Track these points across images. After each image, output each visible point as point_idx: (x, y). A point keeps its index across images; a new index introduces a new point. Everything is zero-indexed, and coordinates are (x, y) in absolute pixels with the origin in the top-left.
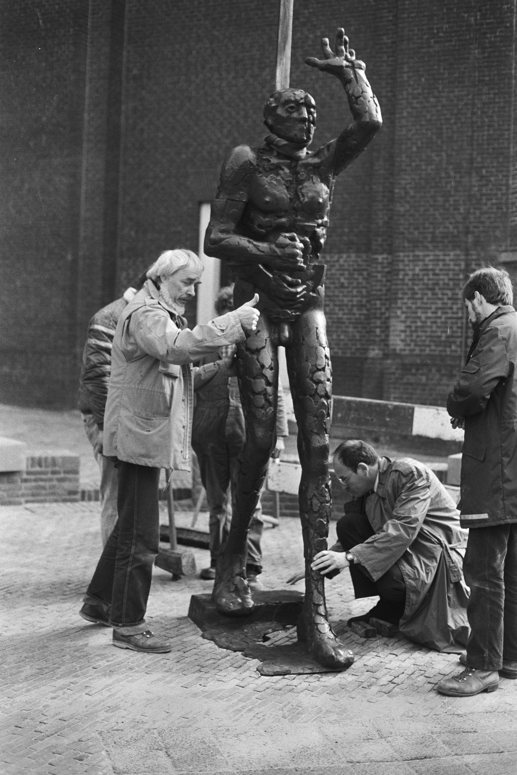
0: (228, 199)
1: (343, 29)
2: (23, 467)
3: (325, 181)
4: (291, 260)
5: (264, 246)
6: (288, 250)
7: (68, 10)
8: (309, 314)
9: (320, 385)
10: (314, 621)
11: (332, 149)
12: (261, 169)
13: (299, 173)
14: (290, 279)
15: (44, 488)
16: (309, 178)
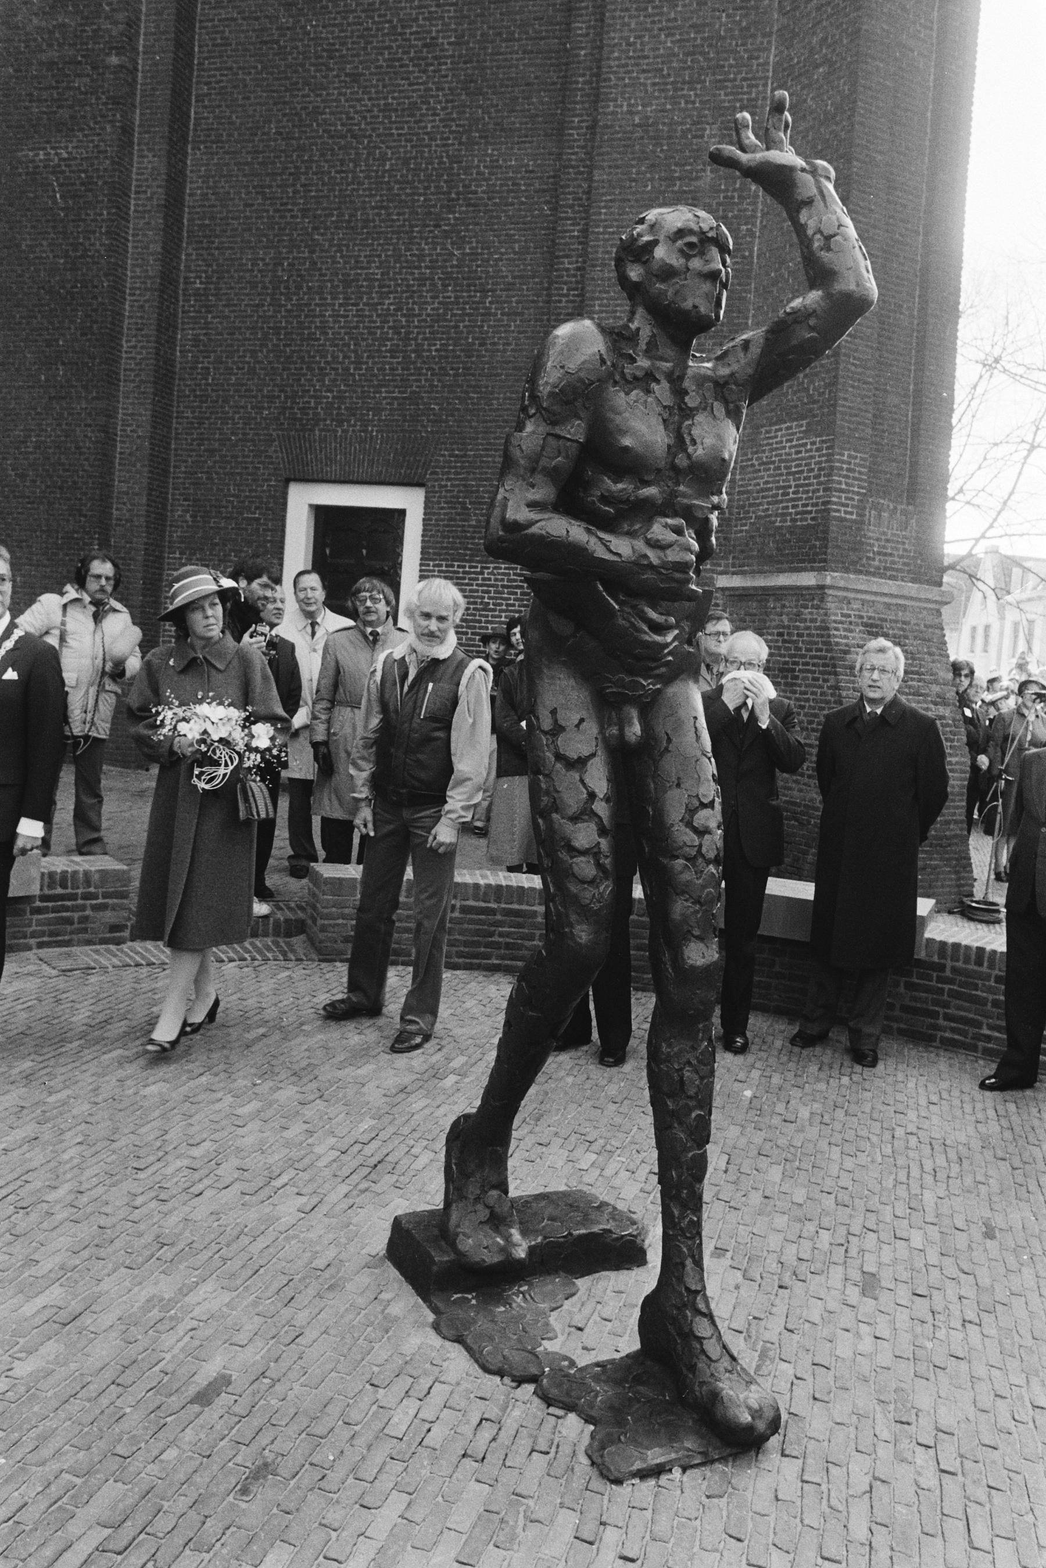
0: (548, 434)
2: (35, 890)
3: (734, 414)
4: (677, 575)
6: (672, 556)
7: (100, 183)
8: (672, 690)
9: (707, 837)
10: (691, 1331)
11: (755, 350)
12: (617, 378)
13: (687, 393)
14: (653, 615)
15: (69, 921)
16: (704, 407)
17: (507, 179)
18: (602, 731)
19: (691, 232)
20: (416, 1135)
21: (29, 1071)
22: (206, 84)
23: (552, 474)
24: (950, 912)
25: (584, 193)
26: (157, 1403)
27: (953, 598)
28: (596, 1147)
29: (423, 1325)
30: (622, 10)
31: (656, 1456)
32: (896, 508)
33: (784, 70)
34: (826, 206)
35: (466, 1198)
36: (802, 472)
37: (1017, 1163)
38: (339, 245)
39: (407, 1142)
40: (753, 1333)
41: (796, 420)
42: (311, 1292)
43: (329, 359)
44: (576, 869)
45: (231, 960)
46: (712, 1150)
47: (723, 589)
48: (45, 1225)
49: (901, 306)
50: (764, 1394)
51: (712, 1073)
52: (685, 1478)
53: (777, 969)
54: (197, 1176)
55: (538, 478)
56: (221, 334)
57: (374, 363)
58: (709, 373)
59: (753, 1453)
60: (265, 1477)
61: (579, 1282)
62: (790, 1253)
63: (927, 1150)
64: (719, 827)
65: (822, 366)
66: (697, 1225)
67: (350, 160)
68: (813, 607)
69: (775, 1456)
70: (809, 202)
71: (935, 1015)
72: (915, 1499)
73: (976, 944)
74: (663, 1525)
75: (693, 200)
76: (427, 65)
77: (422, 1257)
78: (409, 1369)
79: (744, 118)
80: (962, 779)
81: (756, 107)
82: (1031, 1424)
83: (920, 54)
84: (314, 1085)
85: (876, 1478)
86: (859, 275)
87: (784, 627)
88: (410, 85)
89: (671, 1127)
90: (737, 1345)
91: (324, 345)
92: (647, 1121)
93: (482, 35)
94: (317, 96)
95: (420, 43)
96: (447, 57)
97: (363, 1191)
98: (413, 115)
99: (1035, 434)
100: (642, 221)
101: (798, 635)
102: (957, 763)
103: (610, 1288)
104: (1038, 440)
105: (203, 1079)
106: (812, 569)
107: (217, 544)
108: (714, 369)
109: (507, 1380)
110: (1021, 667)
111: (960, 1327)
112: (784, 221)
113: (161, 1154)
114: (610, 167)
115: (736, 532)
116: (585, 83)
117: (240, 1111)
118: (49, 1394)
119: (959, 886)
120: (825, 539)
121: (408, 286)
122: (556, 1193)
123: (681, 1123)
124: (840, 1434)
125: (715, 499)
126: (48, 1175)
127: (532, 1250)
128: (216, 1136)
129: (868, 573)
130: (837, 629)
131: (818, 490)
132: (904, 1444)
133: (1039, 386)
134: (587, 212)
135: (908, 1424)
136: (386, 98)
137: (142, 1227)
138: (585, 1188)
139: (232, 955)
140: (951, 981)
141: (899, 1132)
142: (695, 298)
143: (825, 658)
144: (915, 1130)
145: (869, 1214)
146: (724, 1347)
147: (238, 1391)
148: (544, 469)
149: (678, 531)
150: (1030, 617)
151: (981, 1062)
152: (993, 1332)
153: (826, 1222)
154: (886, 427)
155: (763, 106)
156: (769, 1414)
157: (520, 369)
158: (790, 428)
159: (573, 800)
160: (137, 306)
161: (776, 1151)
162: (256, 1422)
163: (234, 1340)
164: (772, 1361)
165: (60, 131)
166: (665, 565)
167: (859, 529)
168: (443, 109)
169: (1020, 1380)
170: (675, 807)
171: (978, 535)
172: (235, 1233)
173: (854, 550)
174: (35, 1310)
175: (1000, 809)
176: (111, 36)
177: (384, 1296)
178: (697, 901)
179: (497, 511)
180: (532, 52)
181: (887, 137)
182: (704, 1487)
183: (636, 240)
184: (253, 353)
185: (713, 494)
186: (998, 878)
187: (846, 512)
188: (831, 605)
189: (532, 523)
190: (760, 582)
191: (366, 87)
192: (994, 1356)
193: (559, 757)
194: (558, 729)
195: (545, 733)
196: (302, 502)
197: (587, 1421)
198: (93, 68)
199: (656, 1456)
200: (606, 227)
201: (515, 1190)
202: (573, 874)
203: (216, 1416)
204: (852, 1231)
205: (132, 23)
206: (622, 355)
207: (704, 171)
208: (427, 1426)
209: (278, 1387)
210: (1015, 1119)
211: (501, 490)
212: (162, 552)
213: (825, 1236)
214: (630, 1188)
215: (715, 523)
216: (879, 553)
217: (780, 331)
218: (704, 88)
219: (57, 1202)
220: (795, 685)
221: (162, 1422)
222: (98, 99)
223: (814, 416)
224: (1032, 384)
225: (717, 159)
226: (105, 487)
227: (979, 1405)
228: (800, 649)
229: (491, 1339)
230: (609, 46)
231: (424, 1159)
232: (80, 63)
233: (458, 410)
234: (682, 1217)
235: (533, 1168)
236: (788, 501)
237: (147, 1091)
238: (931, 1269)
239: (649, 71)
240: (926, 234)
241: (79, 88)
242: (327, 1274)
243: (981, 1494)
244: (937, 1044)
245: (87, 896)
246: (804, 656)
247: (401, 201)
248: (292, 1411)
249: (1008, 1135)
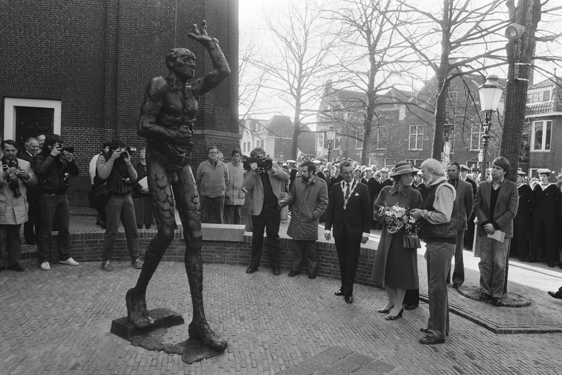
3: (197, 99)
5: (173, 133)
6: (186, 135)
8: (184, 168)
11: (202, 83)
14: (180, 149)
19: (186, 55)
31: (199, 357)
62: (221, 316)
66: (202, 303)
74: (204, 369)
100: (173, 51)
104: (262, 83)
106: (200, 129)
108: (192, 88)
124: (241, 347)
127: (155, 322)
129: (217, 130)
141: (243, 287)
142: (188, 72)
149: (187, 129)
157: (95, 61)
159: (163, 197)
178: (196, 221)
192: (273, 327)
193: (158, 187)
194: (157, 179)
199: (199, 357)
210: (272, 280)
213: (229, 311)
225: (190, 36)
234: (198, 301)
235: (154, 300)
237: (11, 305)
240: (228, 34)
243: (274, 351)
249: (271, 284)
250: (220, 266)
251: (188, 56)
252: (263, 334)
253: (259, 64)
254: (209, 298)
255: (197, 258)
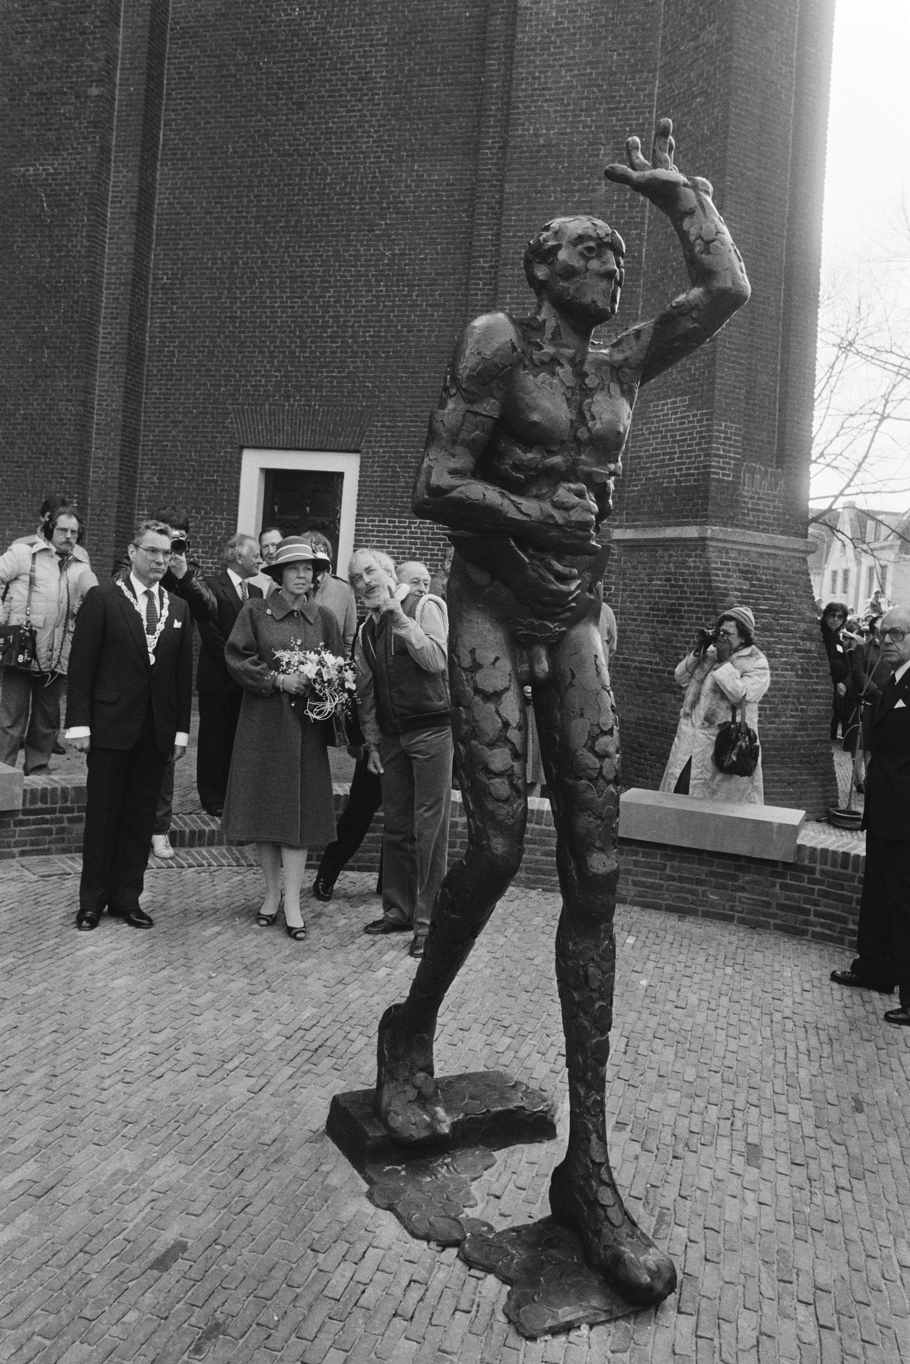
0: (467, 411)
1: (637, 139)
2: (18, 805)
3: (628, 393)
4: (580, 533)
6: (575, 516)
8: (579, 630)
9: (607, 760)
11: (646, 339)
12: (527, 362)
13: (587, 375)
14: (559, 567)
15: (49, 832)
16: (602, 387)
17: (431, 191)
18: (515, 667)
19: (590, 238)
20: (353, 1022)
21: (11, 967)
22: (173, 110)
23: (470, 445)
24: (818, 821)
25: (496, 203)
26: (121, 1269)
27: (816, 545)
28: (509, 1032)
29: (357, 1195)
30: (528, 50)
31: (566, 1314)
32: (766, 472)
33: (666, 100)
34: (706, 216)
35: (397, 1080)
36: (686, 440)
37: (881, 1043)
38: (286, 247)
39: (344, 1028)
40: (651, 1201)
41: (681, 395)
42: (259, 1164)
43: (278, 344)
44: (492, 789)
45: (190, 866)
46: (614, 1036)
47: (618, 541)
48: (22, 1106)
49: (769, 298)
50: (661, 1257)
51: (613, 968)
52: (592, 1335)
53: (668, 871)
54: (158, 1060)
55: (459, 449)
56: (185, 322)
57: (316, 347)
58: (607, 358)
59: (653, 1311)
60: (216, 1337)
61: (497, 1154)
62: (682, 1131)
63: (801, 1033)
64: (617, 752)
65: (704, 349)
66: (601, 1104)
67: (296, 175)
68: (696, 556)
69: (672, 1313)
70: (691, 213)
71: (807, 912)
72: (798, 1353)
73: (841, 850)
75: (590, 210)
76: (363, 95)
77: (360, 1132)
78: (346, 1235)
79: (634, 142)
80: (826, 704)
81: (643, 130)
82: (899, 1283)
83: (783, 87)
84: (263, 977)
85: (761, 1333)
86: (734, 275)
87: (670, 573)
88: (348, 111)
89: (576, 1016)
90: (637, 1210)
91: (273, 332)
92: (556, 1008)
93: (409, 70)
94: (268, 120)
95: (356, 77)
96: (380, 89)
97: (305, 1073)
98: (349, 137)
99: (885, 406)
100: (547, 228)
101: (684, 580)
102: (822, 690)
103: (524, 1159)
104: (887, 411)
105: (165, 973)
106: (695, 524)
107: (180, 503)
108: (610, 355)
109: (433, 1245)
110: (875, 607)
111: (834, 1193)
112: (668, 226)
113: (127, 1040)
114: (519, 181)
115: (629, 492)
116: (497, 110)
117: (196, 1002)
118: (23, 1262)
119: (825, 798)
120: (706, 498)
121: (346, 281)
122: (475, 1074)
123: (586, 1013)
124: (730, 1292)
125: (612, 467)
126: (27, 1060)
127: (454, 1126)
128: (176, 1024)
129: (744, 527)
130: (717, 575)
131: (700, 456)
132: (787, 1302)
133: (888, 366)
134: (499, 219)
135: (791, 1283)
136: (327, 123)
137: (109, 1106)
138: (501, 1069)
139: (191, 861)
140: (820, 882)
141: (777, 1017)
142: (594, 293)
143: (707, 600)
144: (790, 1015)
145: (751, 1091)
146: (626, 1213)
147: (194, 1257)
148: (464, 440)
149: (580, 494)
150: (882, 562)
151: (848, 953)
152: (864, 1198)
153: (714, 1098)
154: (756, 402)
155: (649, 131)
156: (667, 1275)
157: (443, 352)
158: (675, 402)
159: (491, 727)
160: (110, 298)
161: (669, 1034)
162: (208, 1285)
163: (190, 1211)
164: (669, 1225)
165: (48, 150)
166: (569, 524)
167: (736, 489)
168: (376, 132)
169: (888, 1241)
170: (579, 730)
171: (837, 493)
172: (192, 1111)
173: (731, 506)
174: (11, 1184)
175: (860, 730)
176: (92, 71)
177: (324, 1168)
178: (599, 817)
179: (423, 478)
180: (452, 84)
181: (755, 156)
182: (608, 1343)
183: (542, 245)
184: (213, 339)
185: (610, 462)
186: (859, 790)
187: (724, 475)
188: (712, 555)
189: (454, 488)
190: (650, 534)
191: (309, 113)
192: (864, 1218)
193: (477, 691)
194: (476, 666)
195: (465, 670)
196: (253, 465)
197: (504, 1282)
198: (77, 98)
199: (566, 1314)
200: (516, 231)
201: (439, 1072)
202: (490, 794)
203: (173, 1281)
204: (737, 1105)
205: (110, 60)
206: (530, 343)
207: (599, 184)
208: (362, 1287)
209: (229, 1253)
211: (426, 459)
212: (131, 509)
213: (713, 1110)
214: (541, 1067)
215: (612, 487)
216: (753, 510)
217: (667, 322)
218: (599, 114)
219: (33, 1085)
220: (681, 623)
221: (125, 1286)
222: (80, 123)
223: (695, 392)
224: (882, 364)
225: (611, 175)
226: (84, 453)
227: (853, 1265)
228: (686, 593)
229: (418, 1207)
230: (517, 79)
231: (361, 1042)
232: (65, 93)
233: (389, 387)
234: (587, 1097)
235: (456, 1048)
236: (673, 465)
238: (806, 1140)
239: (551, 101)
241: (64, 114)
242: (273, 1148)
243: (856, 1348)
244: (809, 937)
245: (64, 810)
246: (688, 599)
247: (340, 210)
248: (242, 1275)
250: (713, 929)
251: (599, 238)
252: (821, 1242)
253: (884, 357)
254: (658, 1045)
255: (597, 946)
